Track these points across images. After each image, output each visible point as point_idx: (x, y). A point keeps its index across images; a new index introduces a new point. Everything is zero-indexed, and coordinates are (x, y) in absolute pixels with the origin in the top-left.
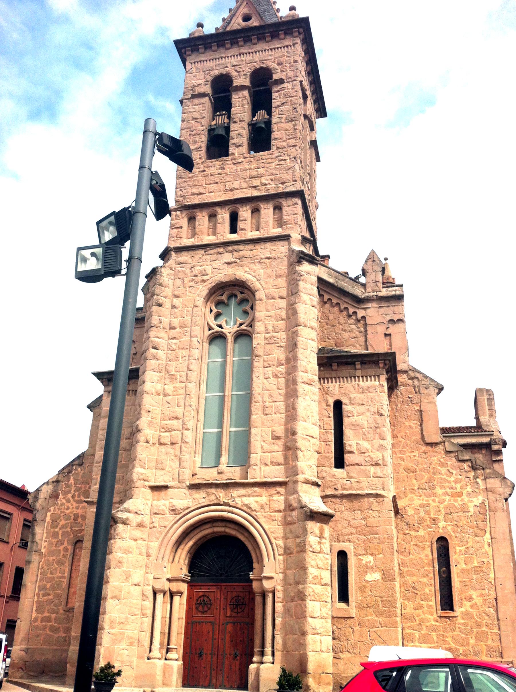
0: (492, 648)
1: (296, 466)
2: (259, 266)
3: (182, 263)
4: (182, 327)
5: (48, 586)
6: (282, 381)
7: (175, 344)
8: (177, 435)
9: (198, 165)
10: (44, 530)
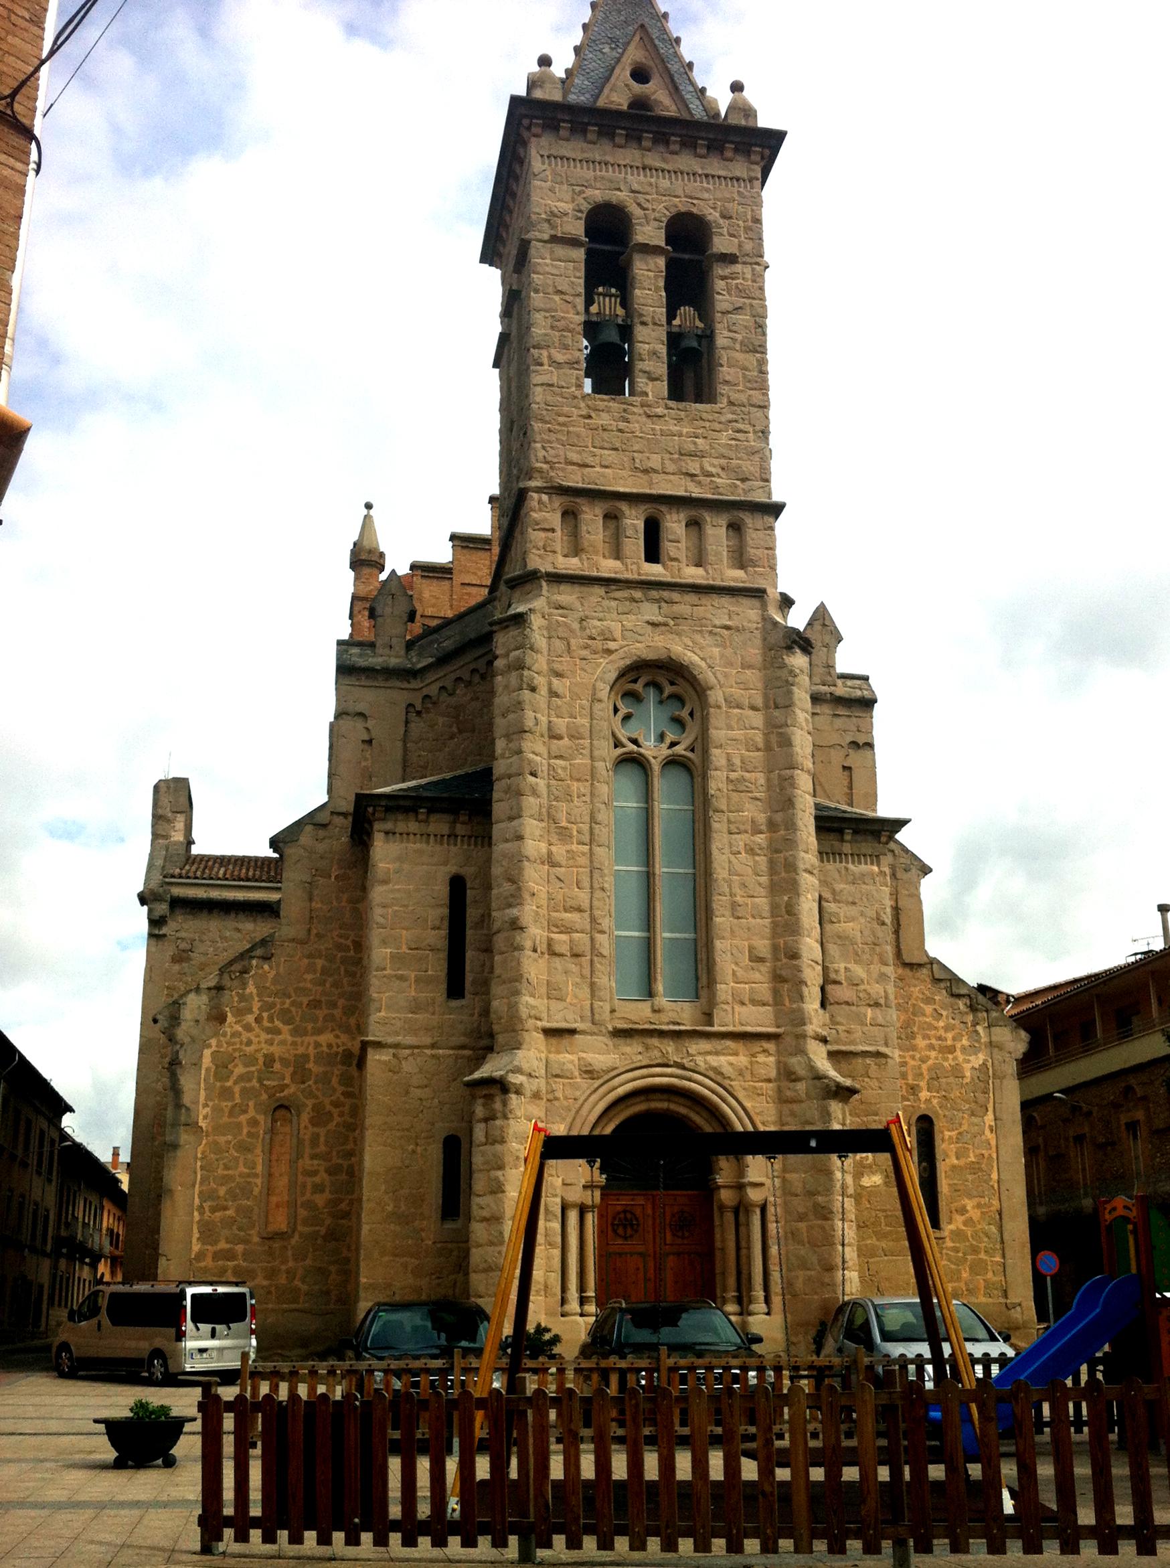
0: (993, 1284)
1: (801, 1010)
2: (709, 640)
3: (563, 608)
4: (572, 736)
5: (222, 1191)
6: (762, 860)
7: (564, 769)
8: (582, 939)
9: (576, 401)
10: (199, 1084)
